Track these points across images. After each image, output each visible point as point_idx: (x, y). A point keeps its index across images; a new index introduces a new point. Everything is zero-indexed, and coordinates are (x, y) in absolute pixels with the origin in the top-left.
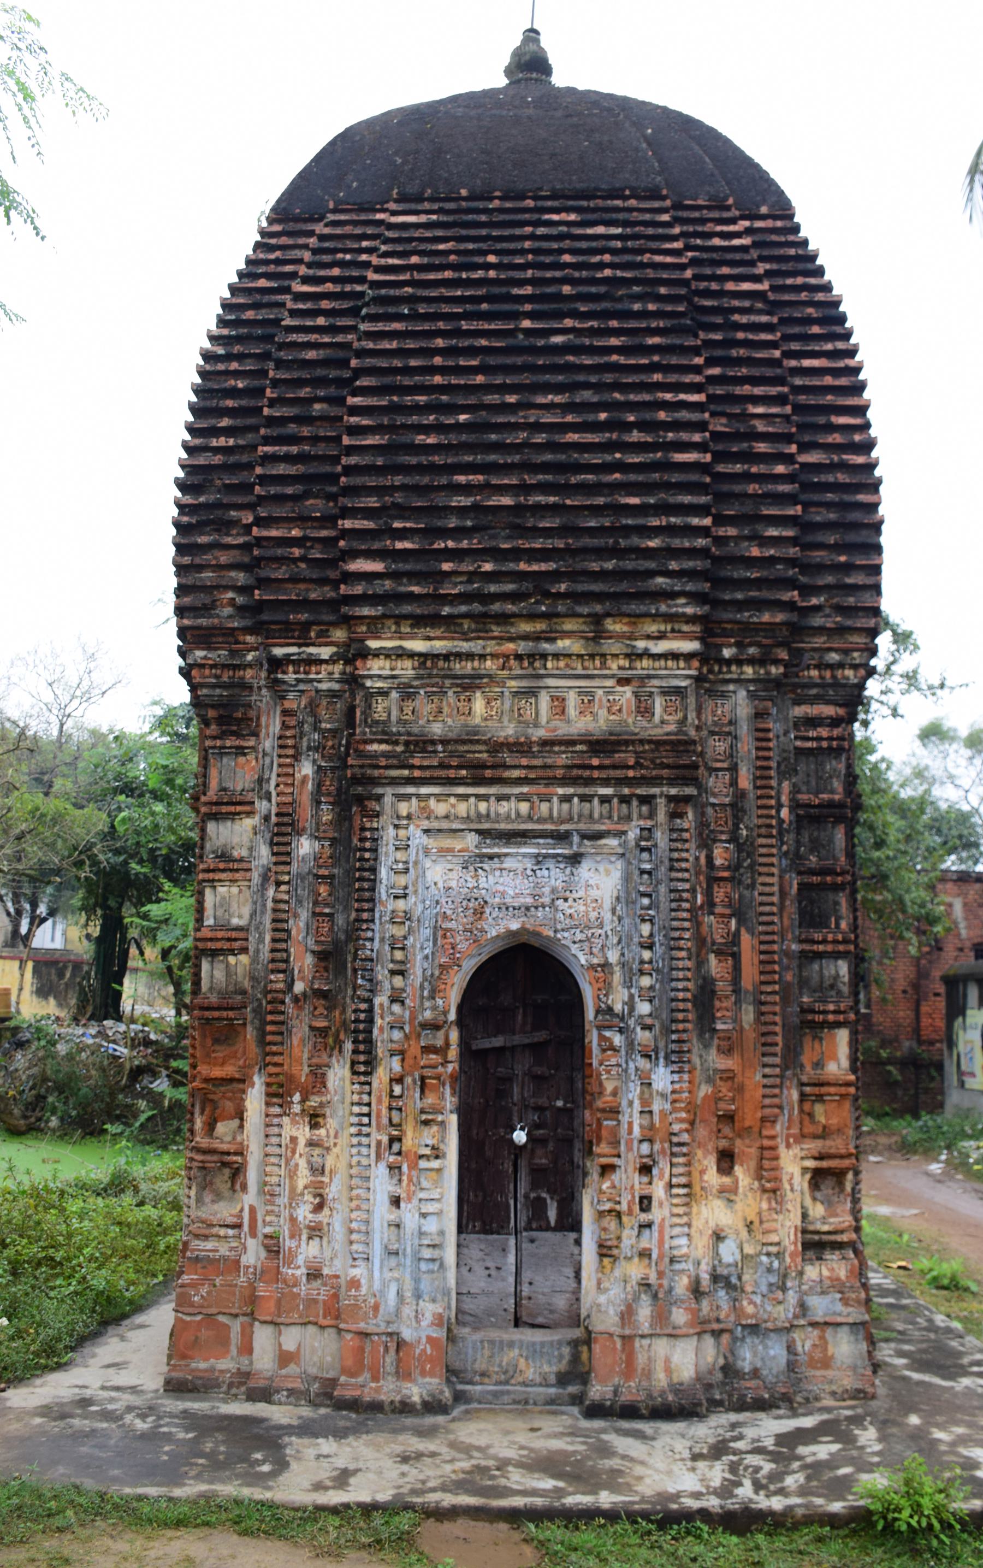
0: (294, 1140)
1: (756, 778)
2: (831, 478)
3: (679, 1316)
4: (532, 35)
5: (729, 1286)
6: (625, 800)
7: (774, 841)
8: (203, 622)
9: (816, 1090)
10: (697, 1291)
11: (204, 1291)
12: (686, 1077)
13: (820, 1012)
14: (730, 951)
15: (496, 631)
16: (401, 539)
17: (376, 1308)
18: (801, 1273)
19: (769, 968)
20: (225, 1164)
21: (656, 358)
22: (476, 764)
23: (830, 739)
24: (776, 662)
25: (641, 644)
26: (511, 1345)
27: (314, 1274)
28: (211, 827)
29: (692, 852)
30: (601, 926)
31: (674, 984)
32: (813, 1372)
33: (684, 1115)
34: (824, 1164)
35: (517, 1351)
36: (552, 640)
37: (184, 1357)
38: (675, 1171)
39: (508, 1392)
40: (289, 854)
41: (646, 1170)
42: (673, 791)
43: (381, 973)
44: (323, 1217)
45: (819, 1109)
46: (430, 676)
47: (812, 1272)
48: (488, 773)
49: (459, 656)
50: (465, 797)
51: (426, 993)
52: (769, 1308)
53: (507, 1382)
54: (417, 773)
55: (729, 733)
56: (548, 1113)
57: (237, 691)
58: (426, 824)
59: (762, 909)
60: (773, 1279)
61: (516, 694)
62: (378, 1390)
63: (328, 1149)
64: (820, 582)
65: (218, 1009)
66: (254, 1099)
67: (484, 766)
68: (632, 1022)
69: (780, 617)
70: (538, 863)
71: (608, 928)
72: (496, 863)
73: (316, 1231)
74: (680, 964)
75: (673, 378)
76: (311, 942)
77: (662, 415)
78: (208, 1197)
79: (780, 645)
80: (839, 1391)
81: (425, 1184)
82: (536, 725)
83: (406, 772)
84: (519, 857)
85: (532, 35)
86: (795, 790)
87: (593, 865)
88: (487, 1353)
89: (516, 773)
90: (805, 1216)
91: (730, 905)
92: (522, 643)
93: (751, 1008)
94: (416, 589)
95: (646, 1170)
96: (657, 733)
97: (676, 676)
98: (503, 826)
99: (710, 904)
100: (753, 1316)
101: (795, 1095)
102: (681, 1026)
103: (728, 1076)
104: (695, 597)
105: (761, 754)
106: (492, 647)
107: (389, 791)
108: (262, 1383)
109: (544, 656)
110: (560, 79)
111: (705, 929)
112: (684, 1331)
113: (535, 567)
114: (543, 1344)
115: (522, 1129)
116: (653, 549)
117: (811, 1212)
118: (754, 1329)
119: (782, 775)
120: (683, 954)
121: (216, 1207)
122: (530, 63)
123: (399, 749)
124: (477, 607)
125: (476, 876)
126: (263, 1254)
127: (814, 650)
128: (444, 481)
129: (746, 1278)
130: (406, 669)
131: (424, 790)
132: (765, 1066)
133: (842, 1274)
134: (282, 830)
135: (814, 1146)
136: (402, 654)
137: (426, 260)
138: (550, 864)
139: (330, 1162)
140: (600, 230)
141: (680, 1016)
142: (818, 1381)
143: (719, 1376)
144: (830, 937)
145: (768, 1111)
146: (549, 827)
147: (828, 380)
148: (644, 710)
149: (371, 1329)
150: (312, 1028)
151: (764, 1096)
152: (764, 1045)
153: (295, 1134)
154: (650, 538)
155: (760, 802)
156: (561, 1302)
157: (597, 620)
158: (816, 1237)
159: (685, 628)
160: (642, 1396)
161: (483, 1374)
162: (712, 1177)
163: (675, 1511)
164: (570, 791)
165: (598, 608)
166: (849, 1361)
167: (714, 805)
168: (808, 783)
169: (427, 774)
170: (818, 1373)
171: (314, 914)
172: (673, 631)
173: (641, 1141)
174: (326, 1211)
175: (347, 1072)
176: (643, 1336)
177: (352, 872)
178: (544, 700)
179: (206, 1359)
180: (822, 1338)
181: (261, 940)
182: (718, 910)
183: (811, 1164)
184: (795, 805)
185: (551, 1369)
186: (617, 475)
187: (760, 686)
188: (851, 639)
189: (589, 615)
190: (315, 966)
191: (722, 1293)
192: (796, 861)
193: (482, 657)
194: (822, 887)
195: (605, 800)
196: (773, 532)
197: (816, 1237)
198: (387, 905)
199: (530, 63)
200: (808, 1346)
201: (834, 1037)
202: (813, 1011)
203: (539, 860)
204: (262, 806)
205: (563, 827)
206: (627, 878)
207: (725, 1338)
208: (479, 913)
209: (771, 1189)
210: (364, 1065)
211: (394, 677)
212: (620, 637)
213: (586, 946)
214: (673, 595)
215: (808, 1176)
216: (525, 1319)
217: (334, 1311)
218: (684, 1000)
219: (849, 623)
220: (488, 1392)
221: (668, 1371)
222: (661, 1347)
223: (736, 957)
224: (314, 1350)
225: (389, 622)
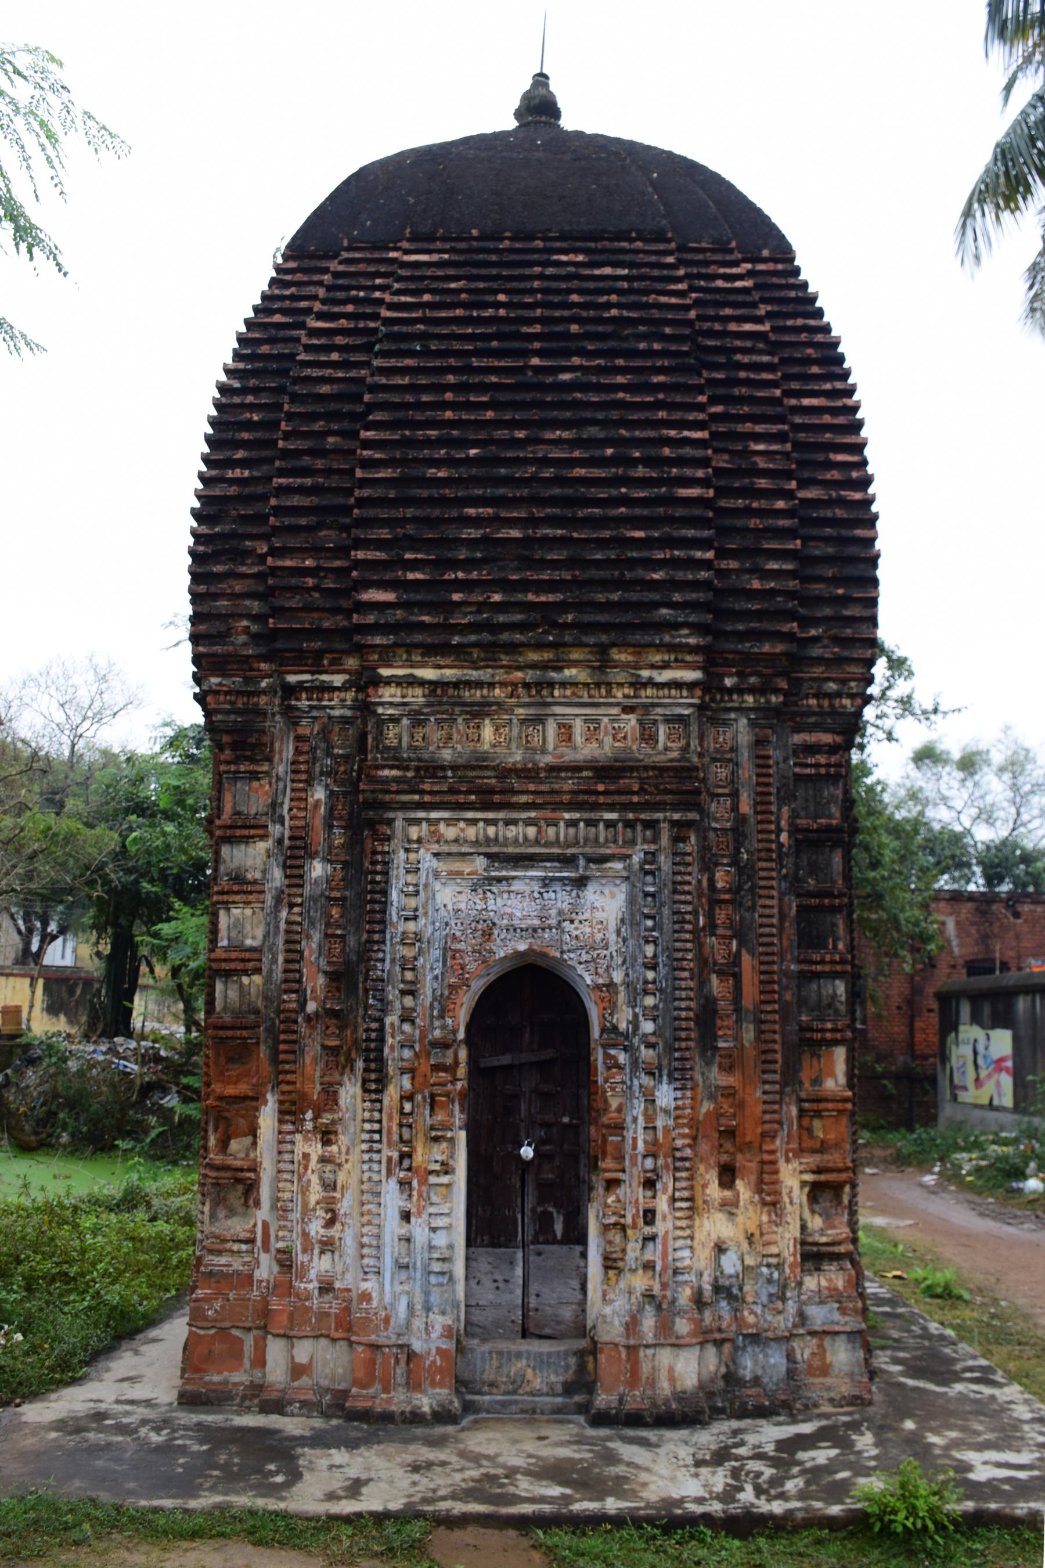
0: (306, 1156)
1: (756, 804)
2: (829, 514)
3: (683, 1326)
4: (541, 79)
5: (731, 1297)
6: (629, 824)
8: (218, 649)
9: (814, 1106)
10: (699, 1301)
11: (217, 1305)
12: (689, 1094)
14: (731, 971)
15: (505, 660)
16: (413, 570)
17: (387, 1320)
18: (800, 1284)
19: (768, 988)
20: (238, 1181)
21: (661, 396)
22: (484, 788)
23: (828, 765)
24: (776, 691)
25: (645, 673)
26: (519, 1355)
27: (326, 1288)
28: (225, 850)
29: (695, 876)
32: (812, 1380)
33: (686, 1131)
34: (823, 1177)
36: (560, 669)
37: (197, 1370)
38: (678, 1185)
40: (301, 876)
41: (649, 1184)
42: (676, 816)
43: (392, 994)
44: (335, 1232)
45: (817, 1124)
46: (440, 704)
47: (811, 1283)
48: (497, 798)
49: (469, 684)
52: (769, 1318)
53: (514, 1392)
54: (427, 798)
55: (730, 760)
56: (555, 1130)
57: (251, 717)
58: (435, 848)
61: (523, 722)
62: (389, 1401)
63: (340, 1165)
66: (267, 1118)
68: (636, 1041)
69: (780, 648)
70: (545, 886)
71: (613, 948)
72: (504, 886)
73: (328, 1246)
74: (683, 984)
76: (323, 962)
78: (221, 1213)
83: (417, 797)
84: (526, 879)
85: (541, 79)
86: (794, 815)
87: (599, 888)
88: (495, 1363)
89: (524, 799)
90: (803, 1228)
91: (731, 927)
92: (530, 672)
93: (751, 1027)
94: (426, 619)
95: (649, 1184)
96: (661, 759)
97: (679, 705)
101: (794, 1111)
103: (729, 1093)
104: (698, 628)
106: (500, 675)
107: (400, 815)
108: (275, 1395)
109: (551, 685)
110: (568, 123)
111: (707, 950)
112: (687, 1340)
113: (543, 598)
117: (809, 1225)
118: (755, 1339)
119: (782, 801)
120: (686, 974)
121: (229, 1222)
122: (539, 106)
123: (410, 774)
124: (486, 637)
125: (485, 899)
126: (276, 1269)
127: (813, 679)
128: (454, 513)
129: (747, 1288)
131: (434, 815)
133: (840, 1284)
134: (295, 854)
136: (412, 682)
139: (341, 1177)
140: (607, 271)
142: (816, 1388)
144: (828, 958)
145: (767, 1126)
146: (556, 850)
148: (648, 737)
149: (382, 1341)
150: (324, 1047)
151: (764, 1112)
152: (764, 1062)
153: (307, 1150)
154: (655, 571)
156: (567, 1313)
157: (602, 650)
159: (688, 658)
160: (647, 1404)
161: (492, 1385)
162: (714, 1191)
165: (604, 638)
167: (715, 830)
168: (806, 808)
169: (437, 799)
170: (817, 1380)
172: (676, 660)
173: (645, 1157)
174: (338, 1226)
175: (358, 1090)
176: (647, 1346)
177: (363, 895)
179: (220, 1372)
180: (820, 1346)
181: (274, 961)
182: (720, 931)
183: (808, 1177)
184: (794, 830)
185: (556, 1379)
186: (623, 510)
189: (595, 645)
191: (724, 1304)
192: (795, 884)
193: (491, 685)
194: (820, 909)
195: (610, 824)
196: (773, 565)
199: (539, 106)
200: (807, 1353)
201: (831, 1054)
202: (811, 1030)
203: (546, 883)
204: (275, 830)
205: (570, 851)
206: (631, 901)
207: (727, 1347)
208: (487, 935)
209: (770, 1199)
210: (375, 1083)
212: (624, 666)
214: (676, 626)
215: (807, 1190)
217: (346, 1322)
218: (687, 1019)
221: (672, 1379)
222: (665, 1357)
223: (737, 977)
224: (325, 1362)
225: (401, 651)
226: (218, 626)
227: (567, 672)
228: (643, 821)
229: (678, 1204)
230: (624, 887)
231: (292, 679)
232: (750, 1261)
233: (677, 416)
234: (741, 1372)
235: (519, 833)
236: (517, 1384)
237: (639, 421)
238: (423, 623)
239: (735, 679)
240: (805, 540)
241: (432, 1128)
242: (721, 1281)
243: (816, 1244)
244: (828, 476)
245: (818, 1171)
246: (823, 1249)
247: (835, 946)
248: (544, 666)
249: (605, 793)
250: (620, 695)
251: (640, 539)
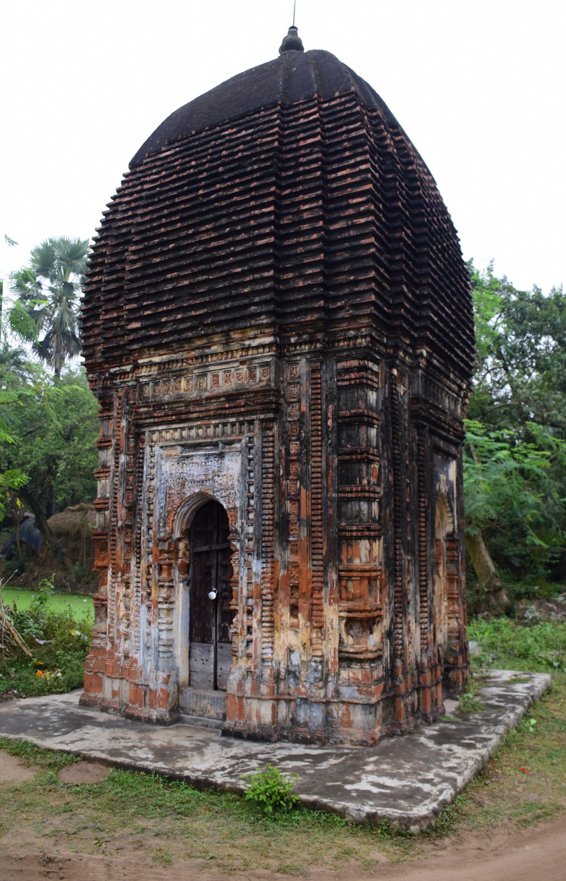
0: (118, 593)
1: (311, 405)
2: (347, 235)
3: (264, 689)
4: (293, 30)
5: (296, 677)
6: (242, 423)
10: (277, 678)
11: (94, 661)
12: (269, 565)
14: (296, 499)
15: (187, 347)
17: (141, 672)
18: (338, 674)
21: (253, 193)
22: (179, 413)
23: (356, 379)
24: (318, 341)
25: (247, 343)
29: (279, 447)
30: (233, 489)
32: (342, 728)
34: (351, 615)
35: (206, 701)
36: (209, 347)
38: (264, 614)
41: (249, 613)
42: (262, 417)
45: (350, 584)
46: (163, 373)
47: (345, 674)
48: (183, 417)
52: (314, 690)
53: (202, 716)
54: (156, 420)
55: (298, 383)
58: (161, 444)
60: (318, 675)
61: (198, 376)
62: (141, 711)
64: (341, 293)
68: (242, 537)
69: (316, 316)
71: (236, 489)
72: (189, 460)
74: (267, 506)
81: (162, 616)
82: (206, 390)
84: (198, 456)
85: (293, 30)
86: (337, 409)
89: (195, 415)
90: (341, 642)
91: (297, 475)
94: (153, 333)
95: (249, 613)
96: (256, 387)
97: (265, 357)
98: (190, 442)
99: (287, 473)
100: (305, 694)
101: (335, 577)
103: (296, 565)
104: (268, 314)
106: (185, 355)
107: (147, 430)
109: (207, 356)
111: (284, 487)
112: (266, 697)
113: (198, 313)
114: (217, 698)
117: (346, 641)
118: (305, 700)
119: (328, 402)
120: (269, 501)
122: (292, 44)
124: (176, 337)
127: (341, 331)
129: (302, 673)
130: (154, 371)
131: (160, 428)
132: (313, 560)
133: (360, 676)
135: (345, 605)
136: (152, 364)
138: (212, 459)
141: (267, 533)
142: (343, 733)
143: (289, 723)
144: (354, 489)
146: (209, 440)
147: (349, 180)
148: (252, 376)
150: (126, 543)
151: (313, 577)
152: (313, 548)
154: (246, 287)
157: (226, 334)
160: (246, 728)
161: (193, 711)
162: (286, 617)
165: (225, 328)
166: (361, 725)
167: (290, 422)
168: (346, 404)
169: (160, 420)
170: (345, 729)
171: (127, 490)
173: (248, 598)
178: (209, 377)
182: (291, 477)
183: (344, 614)
187: (312, 355)
188: (360, 322)
189: (221, 332)
191: (292, 680)
192: (337, 448)
194: (351, 461)
195: (233, 424)
196: (310, 271)
198: (146, 484)
199: (292, 44)
200: (340, 713)
202: (345, 530)
203: (207, 457)
207: (292, 704)
208: (183, 485)
211: (150, 376)
212: (238, 340)
213: (227, 498)
214: (259, 315)
215: (344, 621)
218: (269, 525)
219: (357, 313)
221: (258, 716)
222: (254, 704)
225: (146, 350)
226: (91, 351)
228: (248, 421)
229: (264, 624)
230: (240, 457)
231: (112, 370)
234: (298, 718)
235: (193, 434)
236: (203, 712)
241: (159, 581)
242: (290, 668)
243: (348, 652)
244: (347, 213)
245: (349, 611)
246: (351, 655)
247: (361, 482)
248: (203, 347)
251: (239, 273)
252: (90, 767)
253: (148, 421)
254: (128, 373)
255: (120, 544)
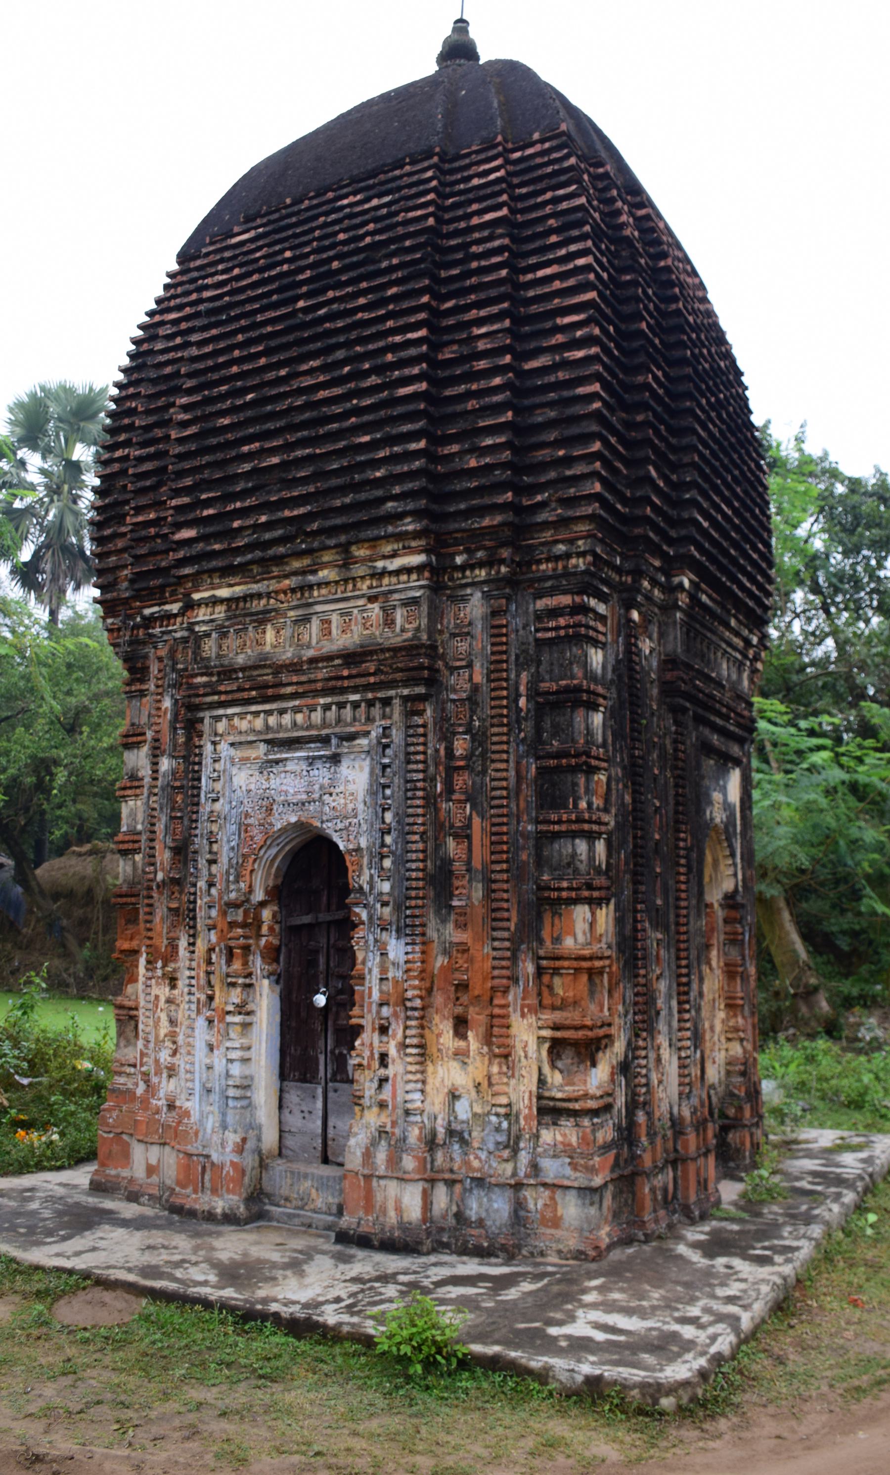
0: (157, 997)
1: (490, 672)
3: (409, 1163)
4: (461, 25)
7: (505, 729)
9: (551, 963)
10: (431, 1143)
13: (554, 889)
14: (464, 835)
15: (276, 571)
17: (196, 1134)
18: (537, 1136)
19: (499, 848)
21: (391, 307)
22: (262, 685)
23: (567, 627)
24: (502, 561)
25: (380, 564)
26: (306, 1176)
30: (355, 816)
31: (408, 865)
32: (543, 1230)
33: (417, 982)
34: (558, 1034)
36: (314, 572)
38: (408, 1032)
39: (298, 1216)
41: (384, 1030)
42: (406, 692)
45: (557, 981)
46: (236, 616)
47: (547, 1136)
48: (270, 692)
50: (256, 714)
51: (231, 878)
52: (495, 1165)
53: (302, 1208)
55: (468, 634)
58: (231, 739)
59: (495, 793)
60: (502, 1138)
61: (296, 622)
65: (126, 896)
67: (267, 687)
69: (498, 519)
70: (311, 764)
71: (360, 817)
72: (280, 768)
74: (414, 847)
75: (401, 322)
76: (169, 840)
77: (390, 357)
79: (503, 545)
80: (565, 1250)
82: (309, 646)
83: (216, 698)
85: (461, 25)
86: (536, 679)
87: (351, 763)
88: (289, 1181)
89: (289, 690)
91: (465, 793)
92: (294, 578)
93: (480, 885)
94: (217, 547)
95: (384, 1030)
96: (396, 641)
97: (411, 588)
98: (281, 735)
99: (449, 790)
100: (479, 1170)
101: (530, 968)
102: (413, 903)
103: (464, 949)
104: (417, 514)
105: (495, 649)
106: (273, 585)
107: (206, 715)
109: (311, 587)
110: (485, 55)
111: (443, 815)
113: (295, 513)
114: (328, 1178)
115: (324, 993)
116: (379, 479)
117: (549, 1080)
118: (480, 1182)
119: (520, 666)
120: (417, 837)
122: (458, 49)
124: (258, 554)
127: (543, 544)
128: (234, 453)
129: (474, 1134)
130: (220, 612)
131: (230, 711)
133: (574, 1140)
135: (548, 1016)
136: (215, 601)
137: (244, 270)
138: (319, 764)
144: (565, 817)
145: (497, 982)
146: (314, 733)
148: (389, 622)
150: (170, 909)
151: (494, 968)
155: (493, 694)
157: (345, 548)
158: (551, 1104)
159: (414, 544)
161: (287, 1199)
162: (447, 1039)
163: (258, 1311)
164: (329, 700)
165: (343, 538)
166: (576, 1223)
167: (454, 701)
168: (551, 672)
169: (229, 697)
170: (549, 1231)
172: (404, 548)
176: (380, 1177)
178: (315, 623)
180: (552, 1198)
184: (534, 693)
186: (353, 419)
187: (493, 586)
189: (335, 546)
190: (173, 859)
191: (456, 1147)
192: (535, 746)
194: (558, 769)
195: (356, 705)
196: (489, 441)
197: (551, 1104)
198: (206, 807)
199: (458, 49)
201: (571, 913)
202: (549, 889)
203: (311, 761)
205: (324, 732)
207: (458, 1188)
208: (269, 810)
209: (503, 1054)
211: (212, 621)
216: (331, 1158)
218: (417, 879)
219: (570, 513)
220: (284, 1213)
221: (399, 1209)
222: (392, 1188)
223: (469, 837)
225: (205, 577)
226: (110, 578)
227: (321, 574)
229: (409, 1050)
232: (478, 1109)
233: (401, 322)
234: (468, 1212)
236: (304, 1202)
237: (372, 335)
238: (214, 551)
239: (465, 556)
240: (517, 411)
241: (228, 975)
243: (553, 1099)
245: (556, 1027)
247: (576, 805)
248: (303, 572)
249: (349, 677)
250: (365, 587)
252: (108, 1296)
253: (209, 699)
254: (175, 616)
255: (160, 912)
